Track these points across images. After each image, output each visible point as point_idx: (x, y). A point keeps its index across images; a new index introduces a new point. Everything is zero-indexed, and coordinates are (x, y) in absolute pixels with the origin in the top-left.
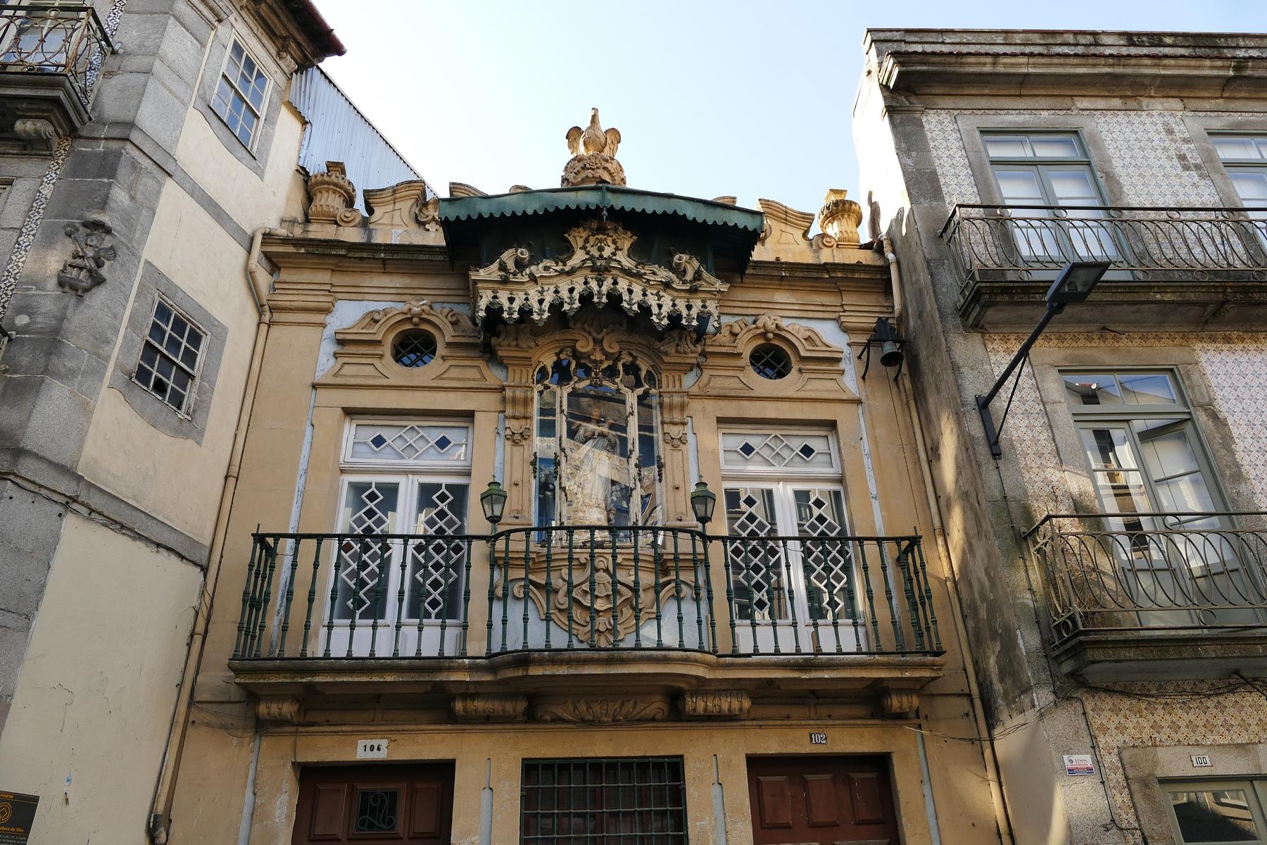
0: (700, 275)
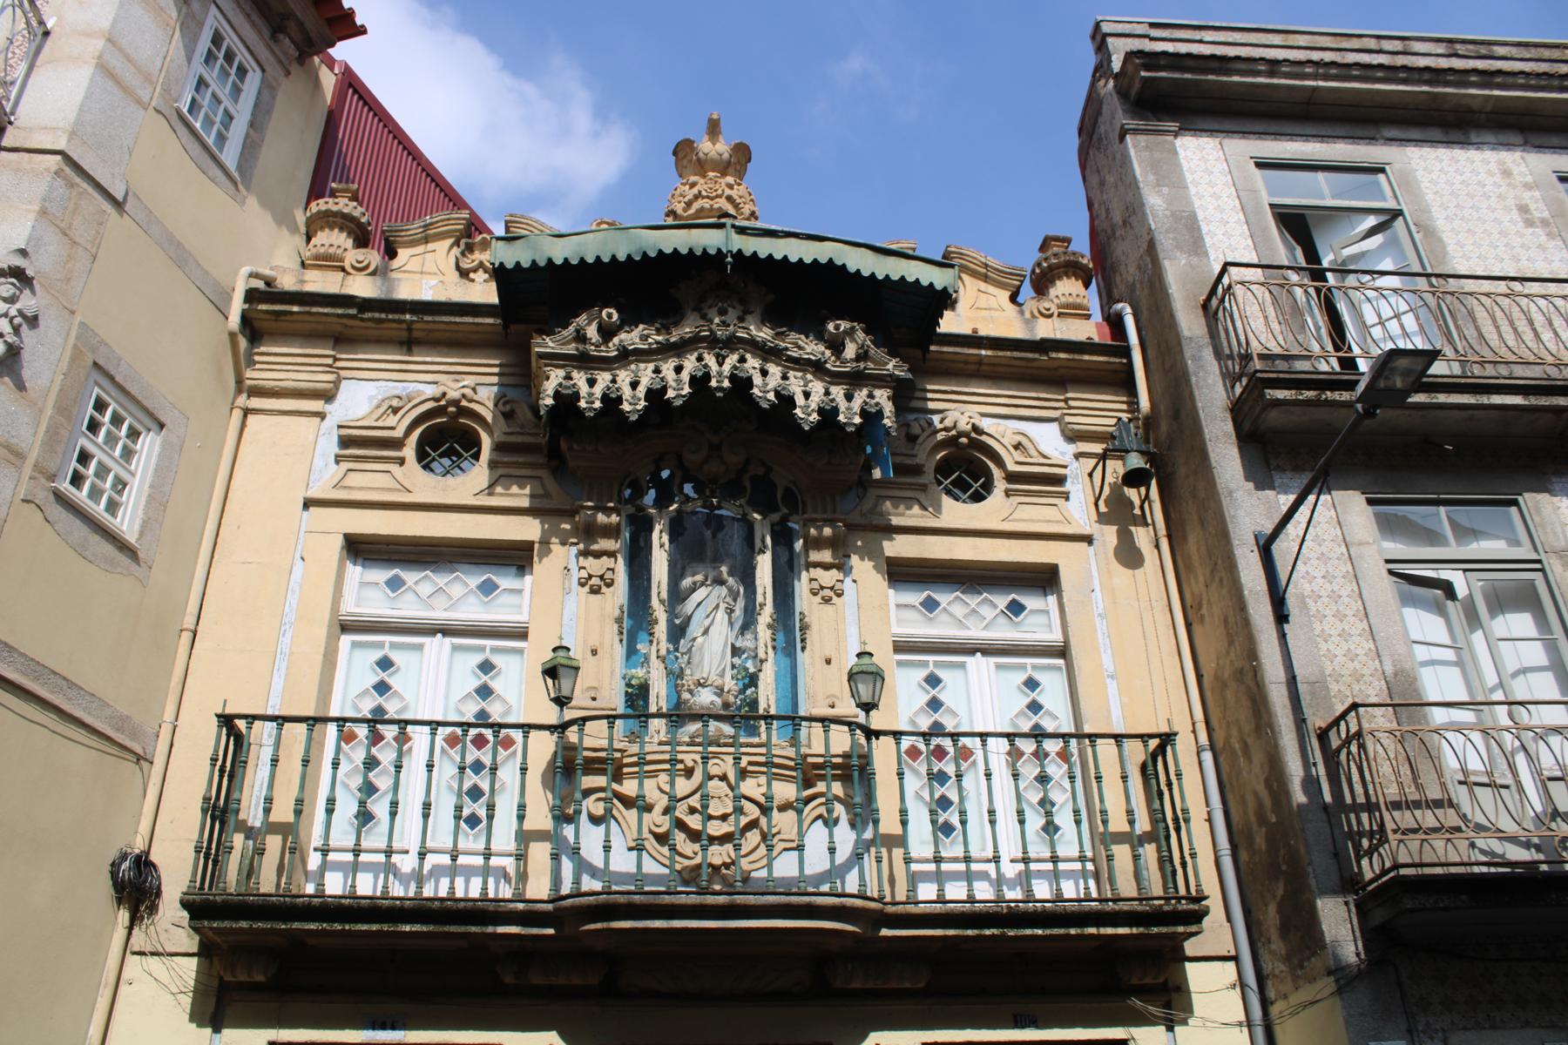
0: (866, 352)
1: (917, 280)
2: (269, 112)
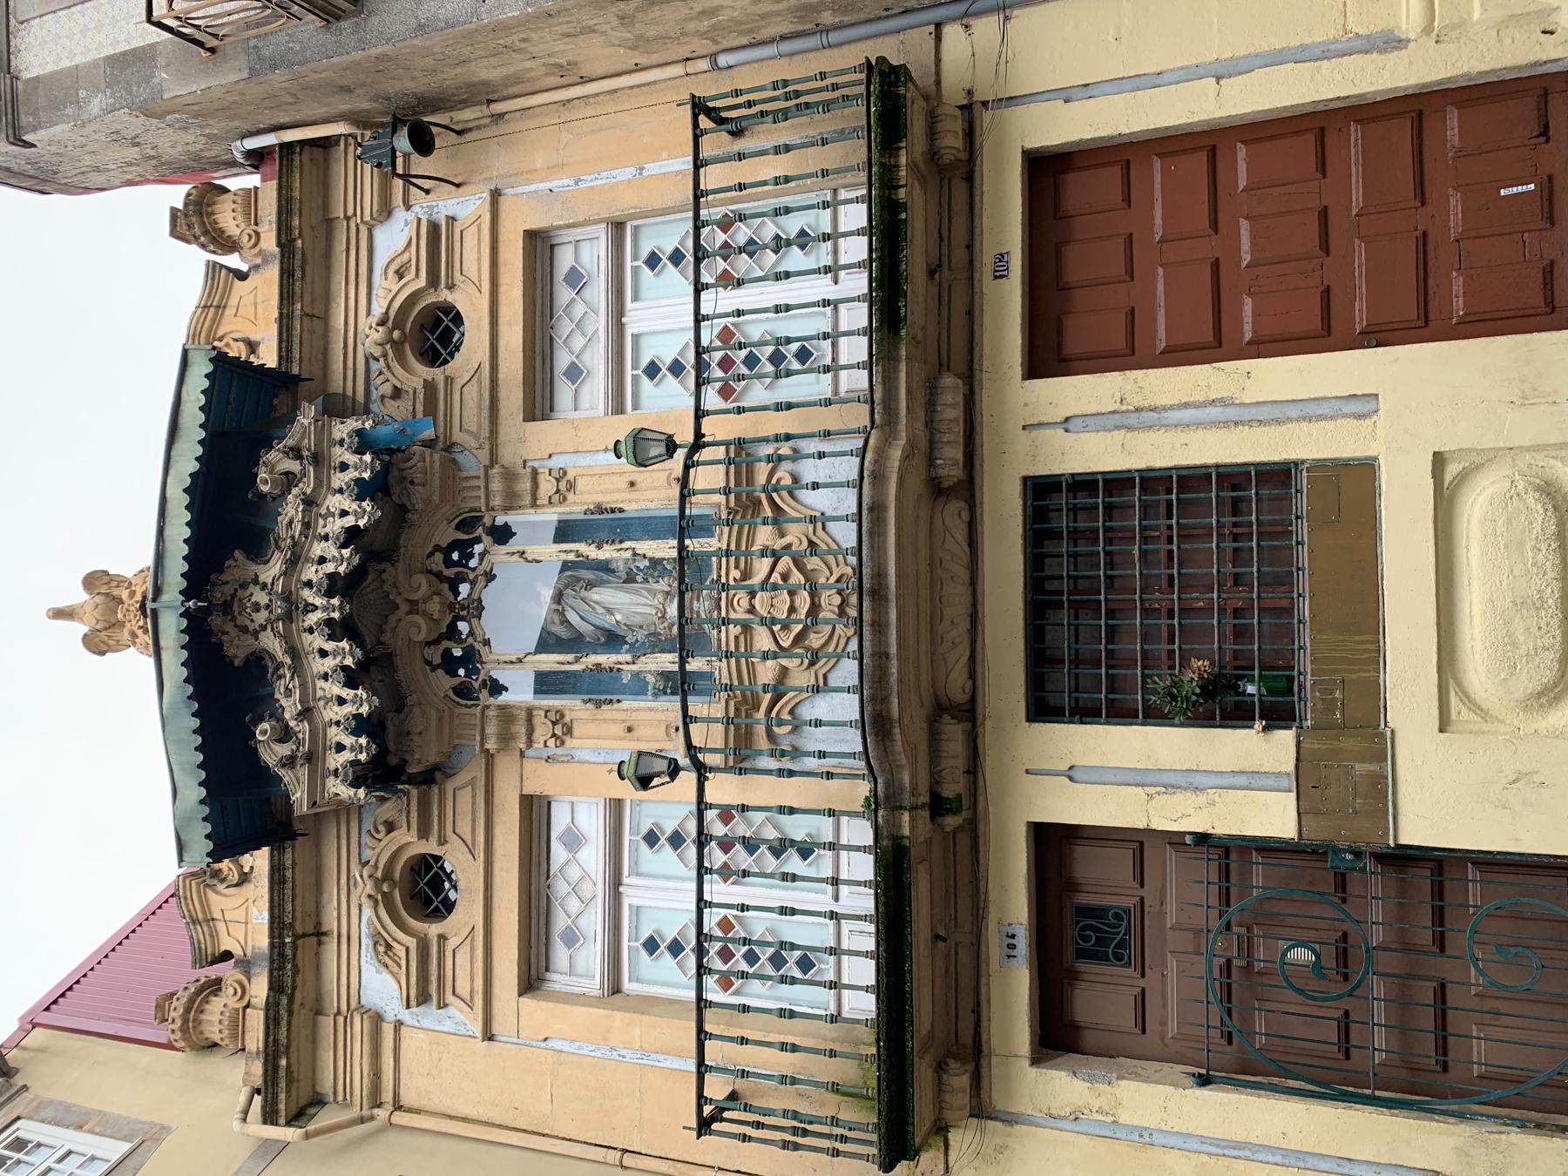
0: (292, 449)
1: (202, 392)
2: (67, 1107)
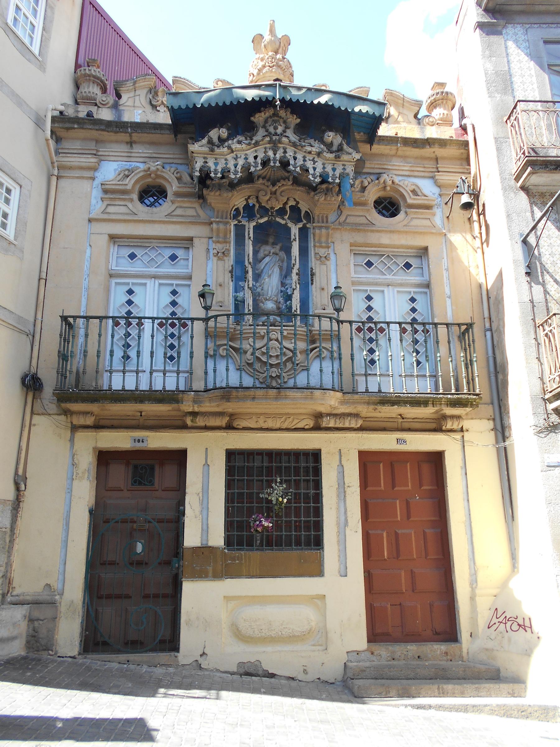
0: (342, 148)
2: (52, 22)
